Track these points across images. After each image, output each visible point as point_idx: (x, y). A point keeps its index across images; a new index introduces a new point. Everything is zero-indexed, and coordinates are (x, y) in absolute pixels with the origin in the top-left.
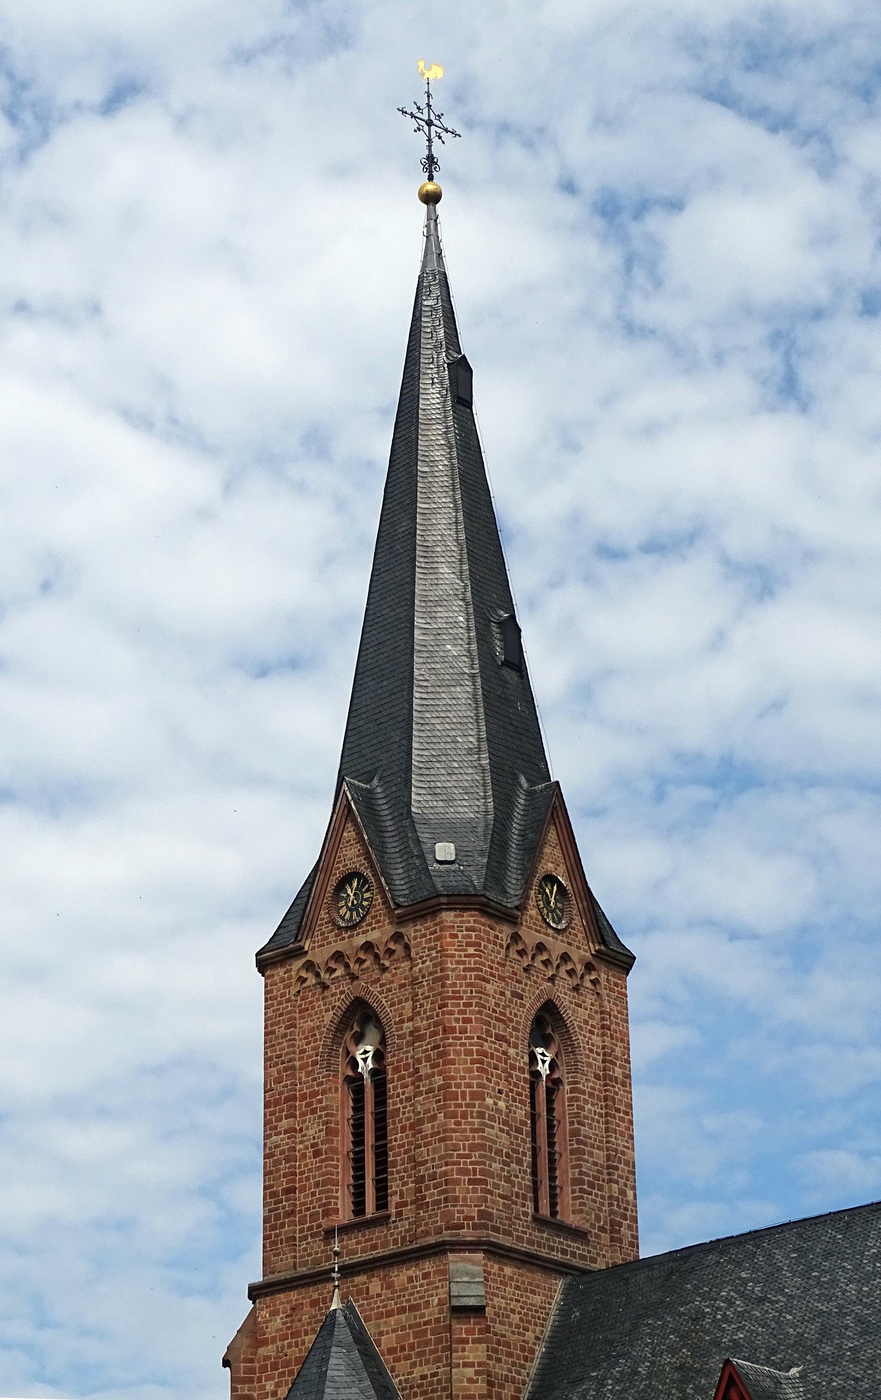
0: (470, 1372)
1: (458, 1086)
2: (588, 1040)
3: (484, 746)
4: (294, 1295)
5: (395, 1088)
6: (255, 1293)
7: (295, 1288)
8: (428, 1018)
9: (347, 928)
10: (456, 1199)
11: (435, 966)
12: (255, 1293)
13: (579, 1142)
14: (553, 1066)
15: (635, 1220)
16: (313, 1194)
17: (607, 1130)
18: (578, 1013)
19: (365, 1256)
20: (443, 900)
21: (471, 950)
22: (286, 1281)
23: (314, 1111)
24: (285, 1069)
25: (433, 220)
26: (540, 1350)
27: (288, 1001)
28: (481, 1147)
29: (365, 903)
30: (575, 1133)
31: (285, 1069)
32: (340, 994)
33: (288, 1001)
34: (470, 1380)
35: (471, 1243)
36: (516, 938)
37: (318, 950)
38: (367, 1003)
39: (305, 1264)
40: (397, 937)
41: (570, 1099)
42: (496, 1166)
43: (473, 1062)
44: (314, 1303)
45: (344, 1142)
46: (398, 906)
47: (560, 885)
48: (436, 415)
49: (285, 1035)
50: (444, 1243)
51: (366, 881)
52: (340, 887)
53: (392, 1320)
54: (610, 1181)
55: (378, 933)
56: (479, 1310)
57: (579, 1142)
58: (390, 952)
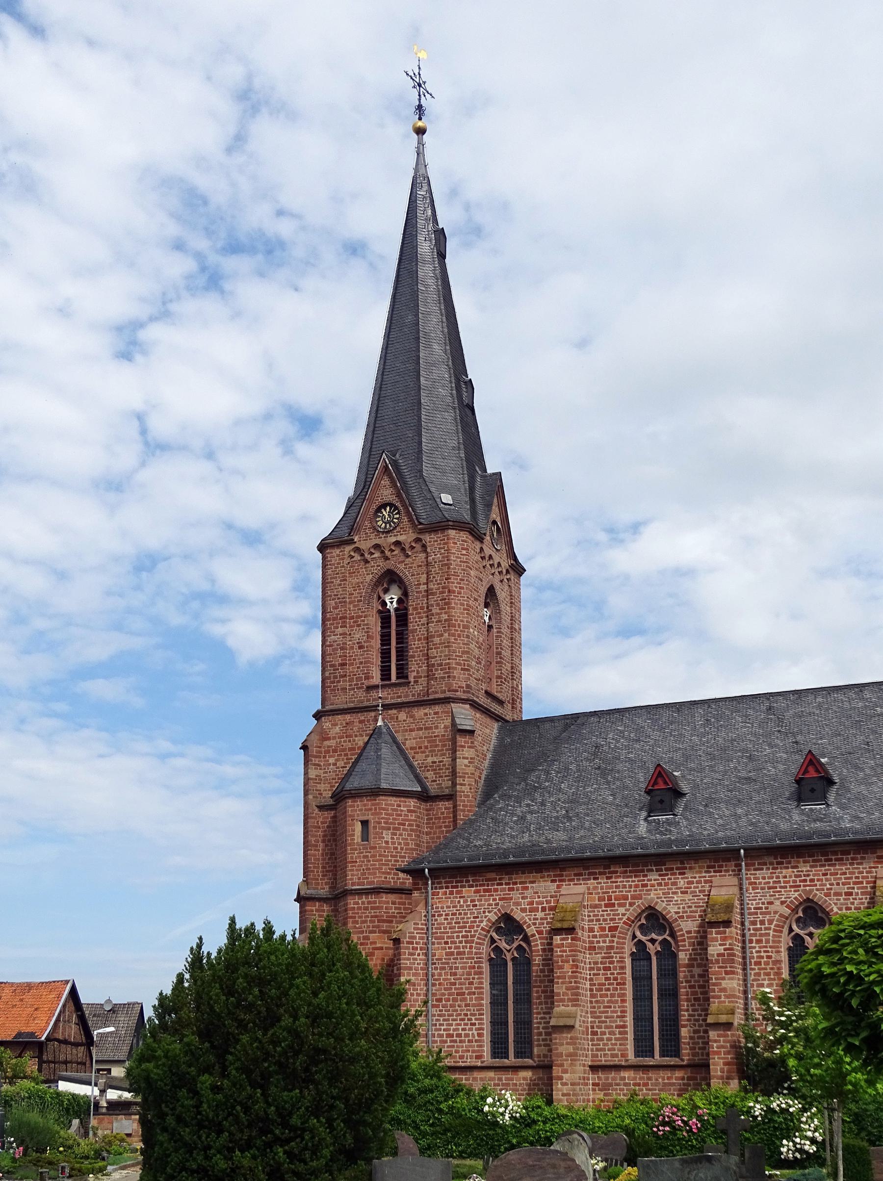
0: (466, 762)
1: (456, 620)
2: (505, 608)
3: (462, 446)
4: (348, 717)
5: (414, 618)
6: (318, 716)
7: (349, 713)
8: (438, 584)
9: (383, 533)
10: (455, 677)
11: (443, 557)
12: (318, 716)
13: (501, 658)
14: (490, 618)
15: (521, 699)
16: (358, 668)
17: (512, 654)
18: (502, 594)
19: (393, 701)
20: (450, 523)
21: (464, 552)
22: (344, 710)
23: (359, 626)
24: (340, 602)
25: (421, 144)
26: (489, 755)
27: (343, 567)
28: (468, 653)
29: (395, 521)
30: (499, 653)
31: (340, 602)
32: (378, 566)
33: (343, 567)
34: (466, 766)
35: (463, 699)
36: (482, 549)
37: (364, 541)
38: (396, 573)
39: (353, 702)
40: (418, 540)
41: (497, 636)
42: (474, 663)
43: (464, 609)
44: (361, 722)
45: (376, 643)
46: (421, 524)
47: (498, 526)
48: (428, 258)
49: (340, 585)
50: (449, 698)
51: (396, 508)
52: (379, 510)
53: (413, 733)
54: (513, 679)
55: (406, 537)
56: (472, 732)
57: (501, 658)
58: (412, 548)
